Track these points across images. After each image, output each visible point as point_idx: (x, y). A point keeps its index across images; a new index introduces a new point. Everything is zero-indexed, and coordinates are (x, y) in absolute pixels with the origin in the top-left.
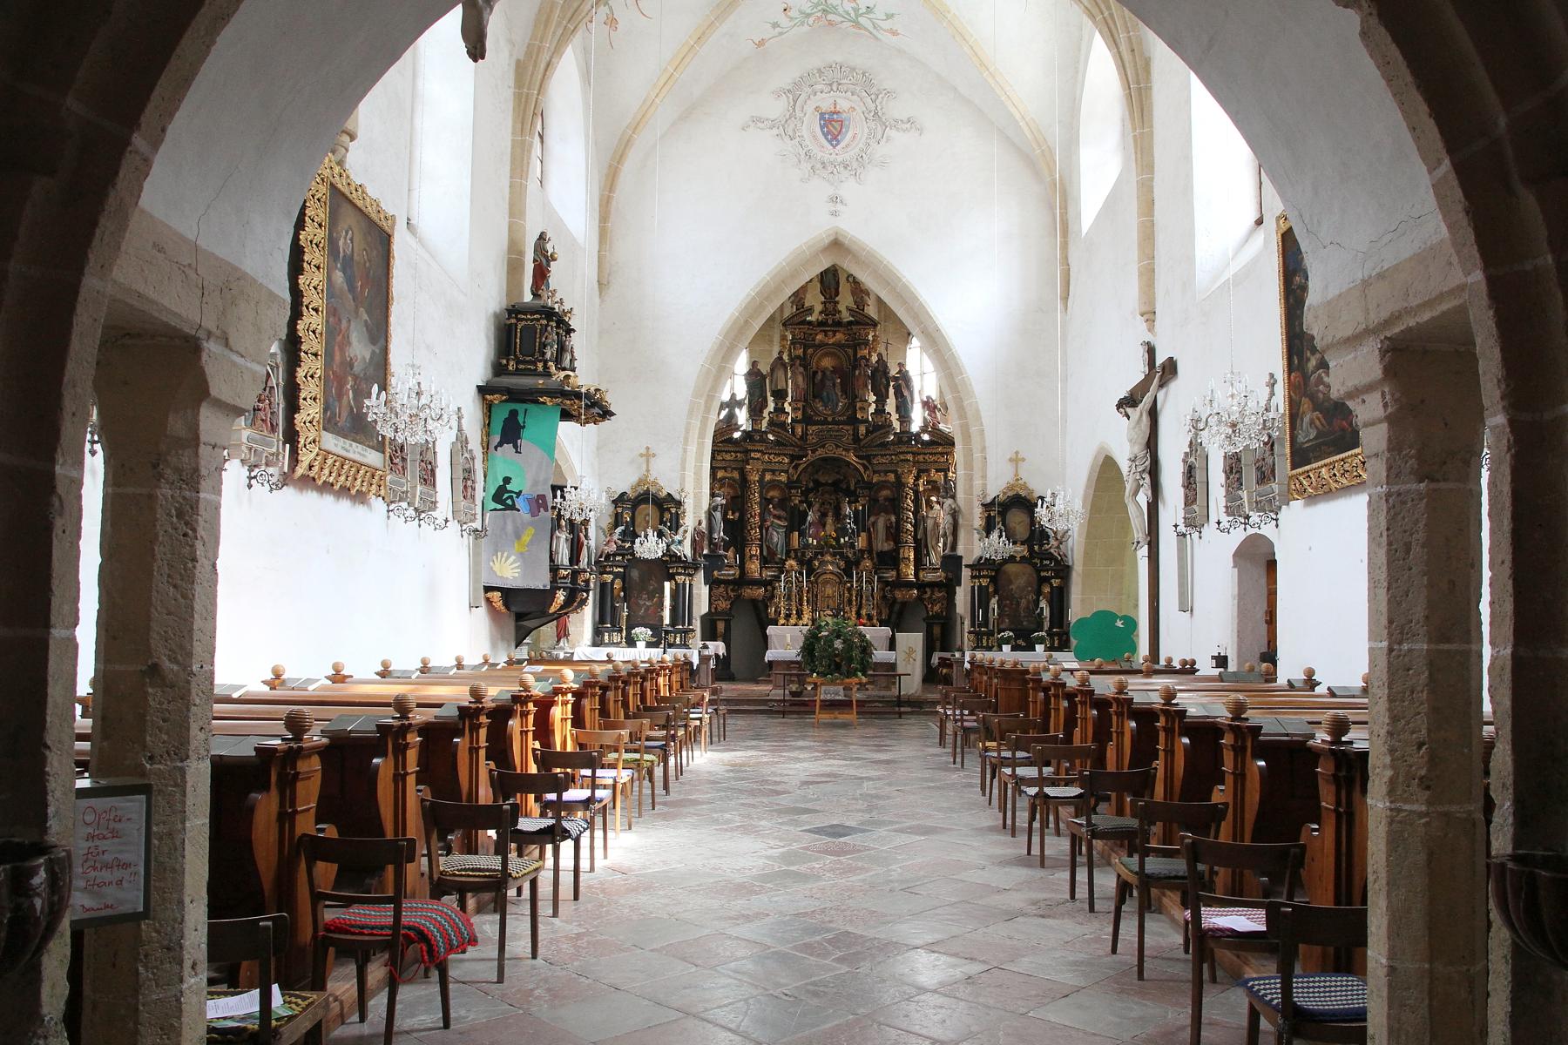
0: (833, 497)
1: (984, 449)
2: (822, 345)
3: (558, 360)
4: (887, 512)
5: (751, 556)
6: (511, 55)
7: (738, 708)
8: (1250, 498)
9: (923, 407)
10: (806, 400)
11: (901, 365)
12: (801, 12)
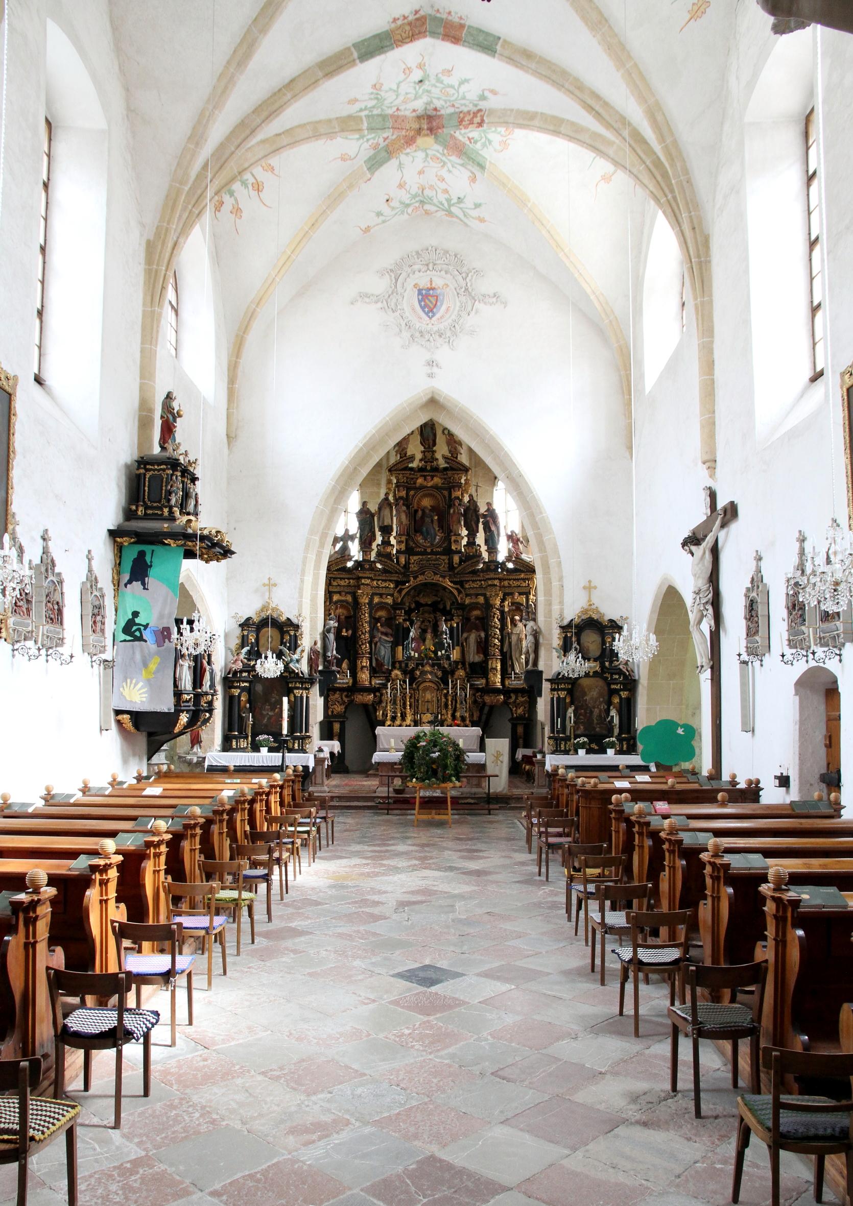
0: (432, 616)
1: (561, 579)
2: (422, 487)
3: (183, 506)
4: (478, 630)
5: (363, 667)
6: (141, 235)
7: (348, 804)
8: (815, 633)
9: (508, 540)
10: (407, 535)
11: (489, 504)
12: (401, 203)
